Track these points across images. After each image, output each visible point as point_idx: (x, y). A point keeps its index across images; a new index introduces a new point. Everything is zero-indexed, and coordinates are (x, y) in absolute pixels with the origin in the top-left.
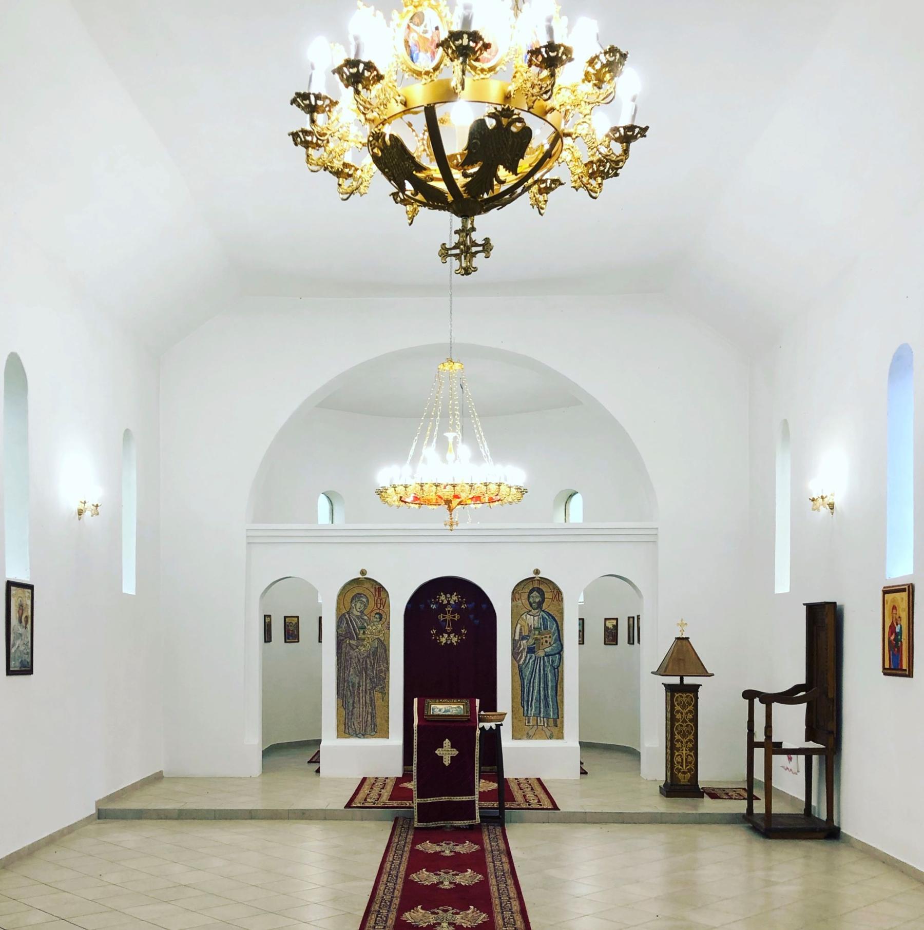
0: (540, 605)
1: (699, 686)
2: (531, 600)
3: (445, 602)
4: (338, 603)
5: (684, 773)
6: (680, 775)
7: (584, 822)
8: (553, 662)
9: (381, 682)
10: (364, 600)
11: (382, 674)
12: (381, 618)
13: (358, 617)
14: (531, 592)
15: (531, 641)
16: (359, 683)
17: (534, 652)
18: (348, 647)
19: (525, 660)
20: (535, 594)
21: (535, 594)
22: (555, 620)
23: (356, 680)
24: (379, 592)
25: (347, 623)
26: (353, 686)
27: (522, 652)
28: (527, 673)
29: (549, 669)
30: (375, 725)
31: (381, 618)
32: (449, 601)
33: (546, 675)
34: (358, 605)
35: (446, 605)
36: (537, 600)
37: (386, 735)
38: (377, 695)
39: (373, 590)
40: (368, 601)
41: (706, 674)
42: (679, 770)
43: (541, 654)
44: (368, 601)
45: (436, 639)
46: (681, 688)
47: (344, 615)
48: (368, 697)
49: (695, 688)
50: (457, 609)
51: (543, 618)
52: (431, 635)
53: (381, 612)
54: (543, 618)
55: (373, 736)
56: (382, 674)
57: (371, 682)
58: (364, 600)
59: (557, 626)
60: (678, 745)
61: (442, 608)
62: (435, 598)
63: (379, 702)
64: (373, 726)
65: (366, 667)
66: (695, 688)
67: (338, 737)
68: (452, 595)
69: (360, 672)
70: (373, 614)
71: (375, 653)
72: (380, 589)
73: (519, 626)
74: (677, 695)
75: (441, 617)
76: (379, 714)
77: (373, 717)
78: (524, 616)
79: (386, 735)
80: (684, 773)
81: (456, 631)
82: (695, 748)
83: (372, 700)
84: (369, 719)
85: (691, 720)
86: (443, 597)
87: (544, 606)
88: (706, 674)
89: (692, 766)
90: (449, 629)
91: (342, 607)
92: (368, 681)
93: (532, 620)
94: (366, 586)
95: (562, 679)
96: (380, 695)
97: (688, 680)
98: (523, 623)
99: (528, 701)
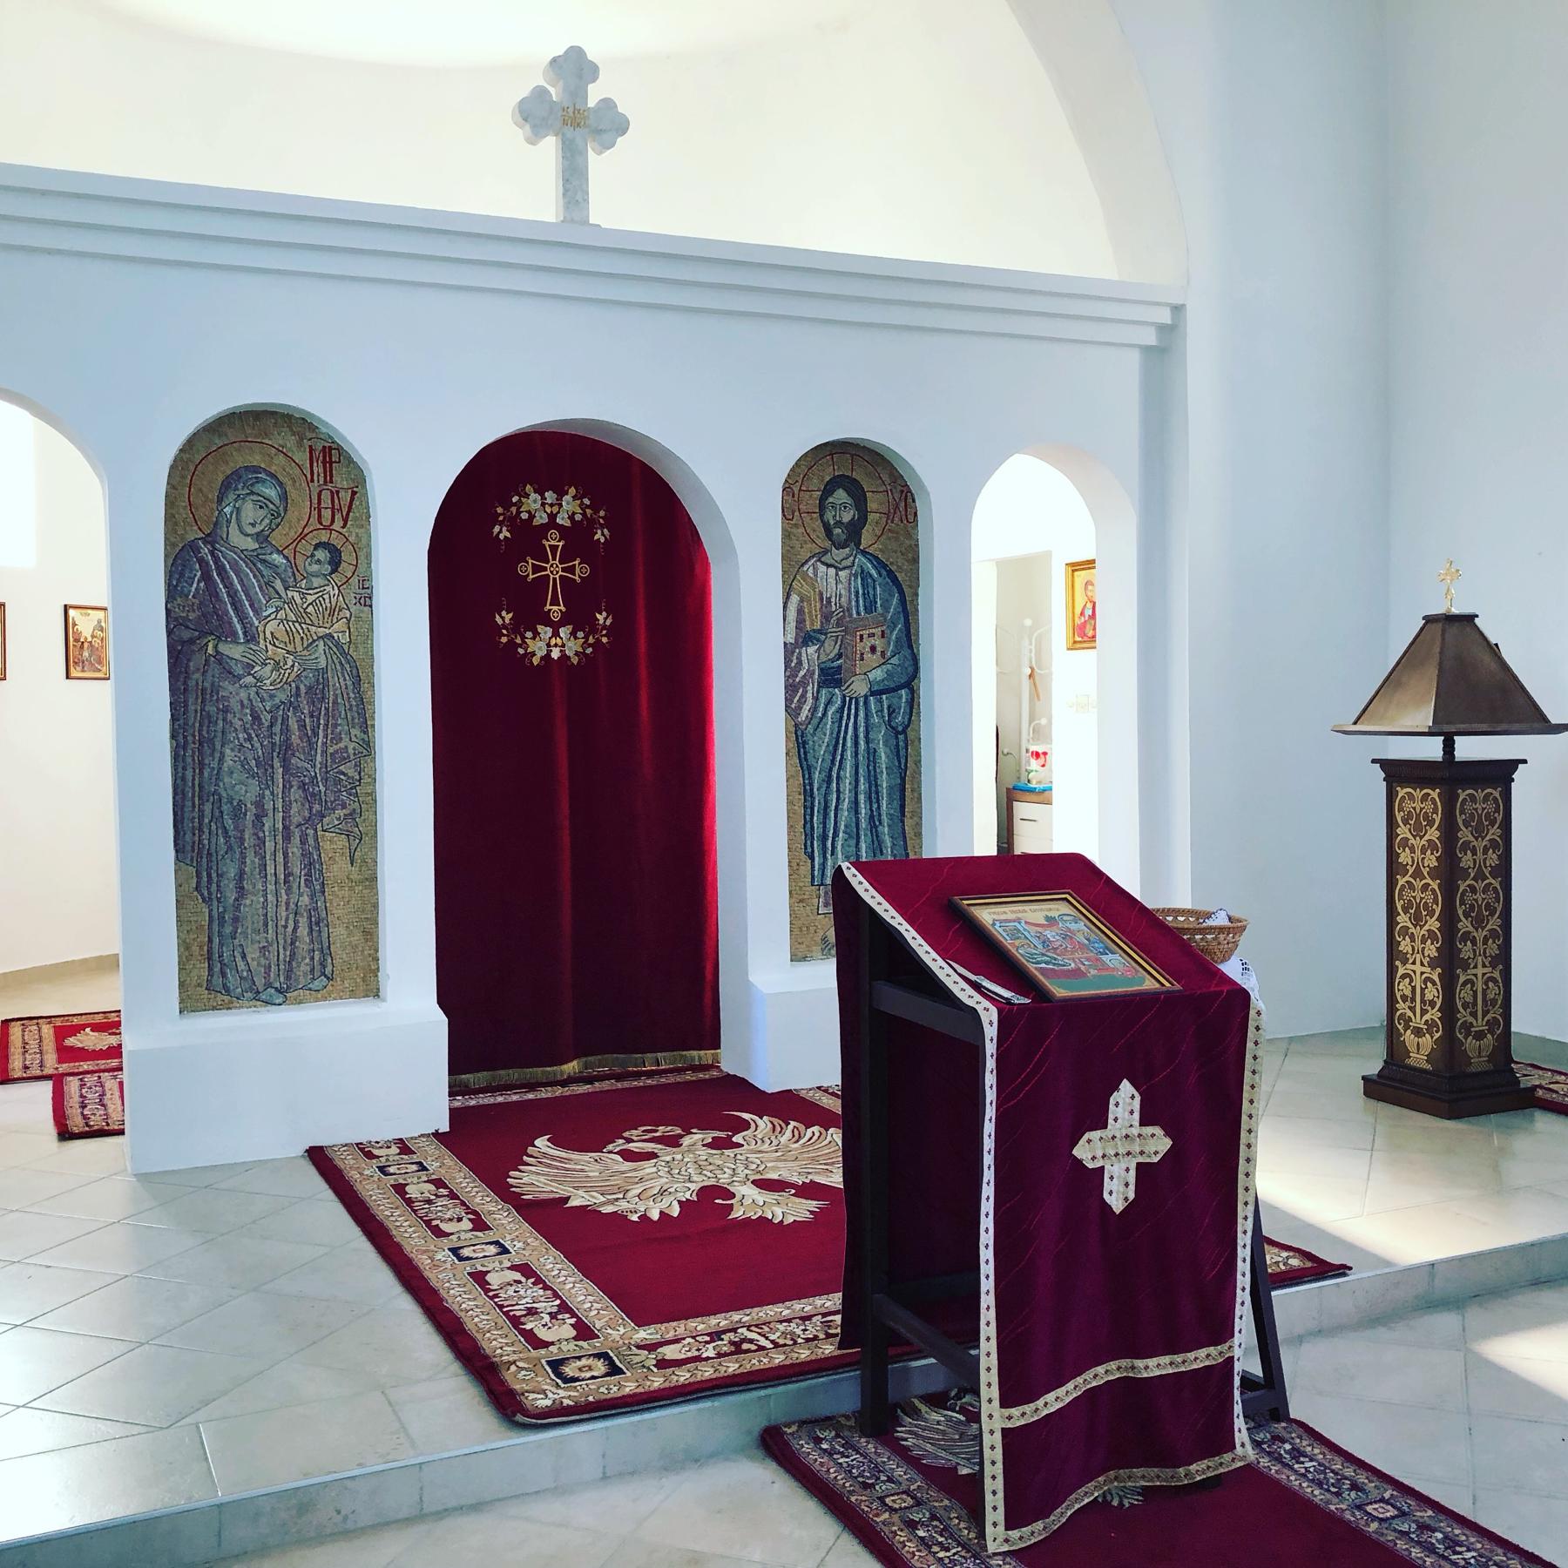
0: (854, 531)
1: (1513, 764)
2: (829, 516)
3: (541, 519)
4: (170, 502)
5: (1480, 1036)
6: (1470, 1044)
7: (1538, 1283)
8: (892, 711)
9: (347, 794)
10: (271, 492)
11: (349, 769)
12: (335, 563)
13: (254, 559)
14: (828, 490)
15: (831, 648)
16: (259, 804)
17: (838, 683)
18: (214, 669)
19: (814, 709)
20: (841, 496)
21: (841, 496)
22: (895, 581)
23: (248, 791)
24: (328, 463)
25: (206, 577)
26: (238, 812)
27: (804, 684)
28: (820, 747)
29: (880, 735)
30: (326, 952)
31: (335, 563)
32: (552, 517)
33: (872, 754)
34: (250, 512)
35: (544, 529)
36: (847, 517)
37: (368, 986)
38: (333, 845)
39: (302, 457)
40: (284, 497)
41: (1533, 720)
42: (1467, 1027)
43: (859, 687)
44: (284, 497)
45: (512, 645)
46: (1449, 775)
47: (192, 546)
48: (295, 850)
49: (1501, 773)
50: (577, 539)
51: (864, 575)
52: (497, 630)
53: (336, 541)
54: (864, 575)
55: (320, 995)
56: (349, 769)
57: (310, 797)
58: (271, 492)
59: (903, 601)
60: (1466, 951)
61: (529, 537)
62: (507, 505)
63: (337, 868)
64: (326, 960)
65: (287, 745)
66: (1501, 773)
67: (189, 1003)
68: (561, 494)
69: (265, 764)
70: (306, 547)
71: (318, 691)
72: (330, 456)
73: (795, 598)
74: (1435, 794)
75: (527, 569)
76: (339, 906)
77: (317, 923)
78: (808, 569)
79: (368, 986)
80: (1480, 1036)
81: (578, 619)
82: (1503, 959)
83: (312, 864)
84: (303, 931)
85: (1494, 875)
86: (533, 501)
87: (866, 538)
88: (1533, 720)
89: (1495, 1013)
90: (556, 611)
91: (185, 513)
92: (296, 794)
93: (833, 582)
94: (277, 440)
95: (918, 763)
96: (341, 842)
97: (1469, 748)
98: (807, 590)
99: (824, 838)
